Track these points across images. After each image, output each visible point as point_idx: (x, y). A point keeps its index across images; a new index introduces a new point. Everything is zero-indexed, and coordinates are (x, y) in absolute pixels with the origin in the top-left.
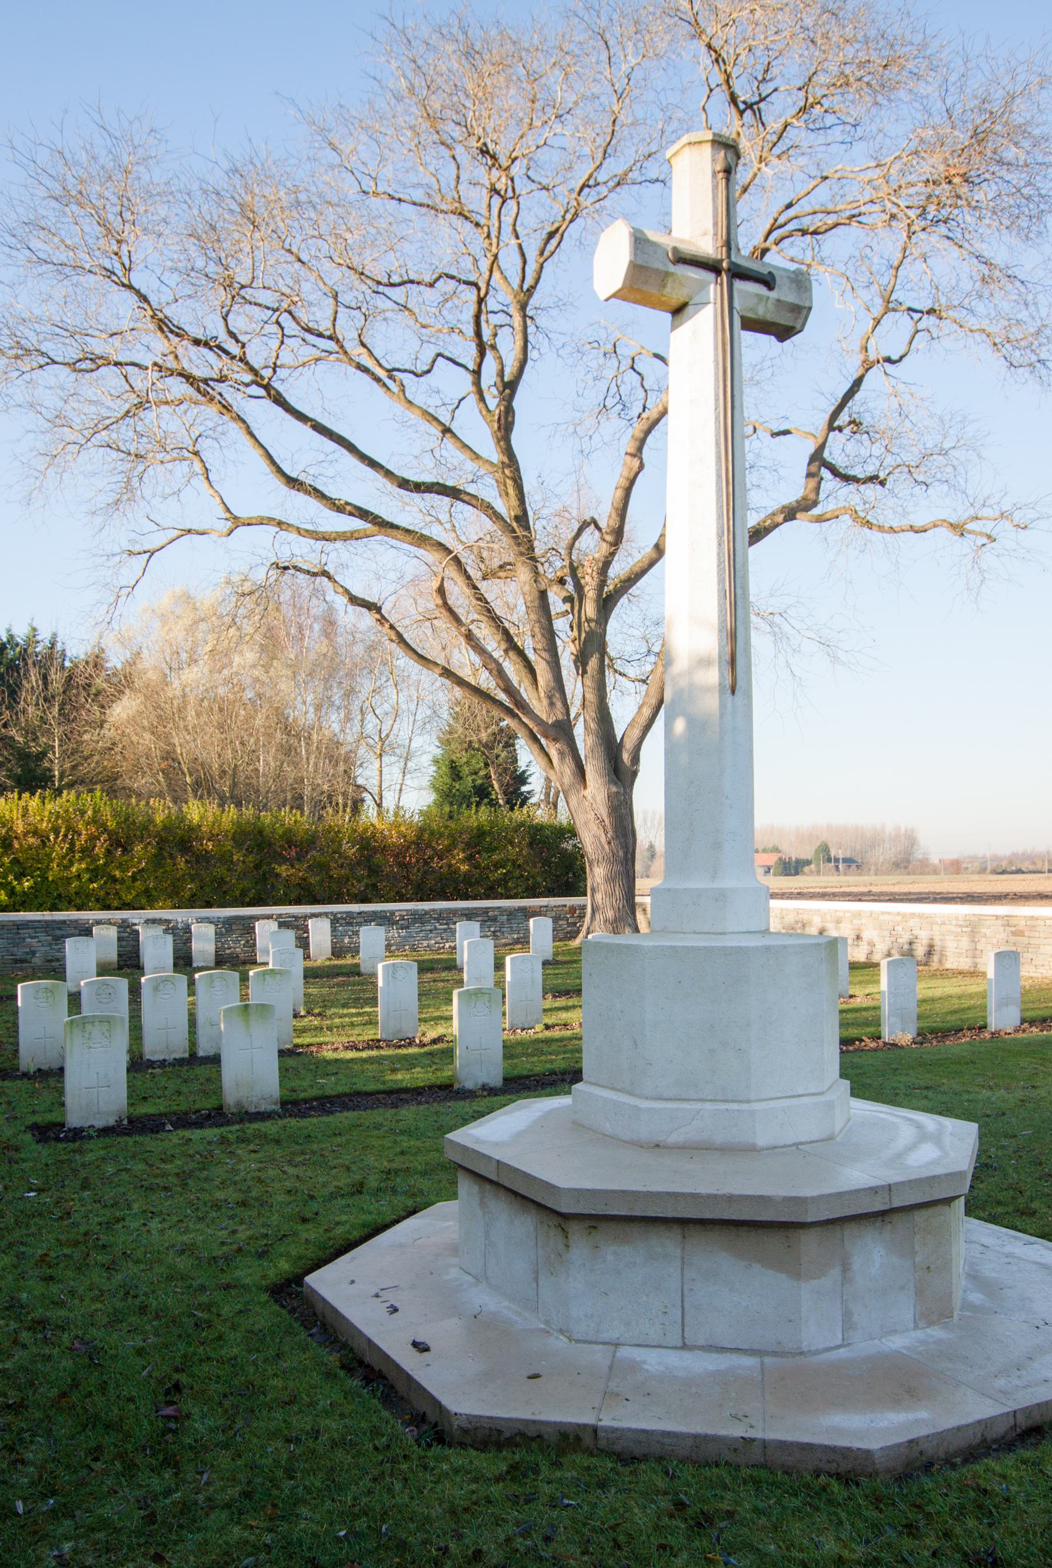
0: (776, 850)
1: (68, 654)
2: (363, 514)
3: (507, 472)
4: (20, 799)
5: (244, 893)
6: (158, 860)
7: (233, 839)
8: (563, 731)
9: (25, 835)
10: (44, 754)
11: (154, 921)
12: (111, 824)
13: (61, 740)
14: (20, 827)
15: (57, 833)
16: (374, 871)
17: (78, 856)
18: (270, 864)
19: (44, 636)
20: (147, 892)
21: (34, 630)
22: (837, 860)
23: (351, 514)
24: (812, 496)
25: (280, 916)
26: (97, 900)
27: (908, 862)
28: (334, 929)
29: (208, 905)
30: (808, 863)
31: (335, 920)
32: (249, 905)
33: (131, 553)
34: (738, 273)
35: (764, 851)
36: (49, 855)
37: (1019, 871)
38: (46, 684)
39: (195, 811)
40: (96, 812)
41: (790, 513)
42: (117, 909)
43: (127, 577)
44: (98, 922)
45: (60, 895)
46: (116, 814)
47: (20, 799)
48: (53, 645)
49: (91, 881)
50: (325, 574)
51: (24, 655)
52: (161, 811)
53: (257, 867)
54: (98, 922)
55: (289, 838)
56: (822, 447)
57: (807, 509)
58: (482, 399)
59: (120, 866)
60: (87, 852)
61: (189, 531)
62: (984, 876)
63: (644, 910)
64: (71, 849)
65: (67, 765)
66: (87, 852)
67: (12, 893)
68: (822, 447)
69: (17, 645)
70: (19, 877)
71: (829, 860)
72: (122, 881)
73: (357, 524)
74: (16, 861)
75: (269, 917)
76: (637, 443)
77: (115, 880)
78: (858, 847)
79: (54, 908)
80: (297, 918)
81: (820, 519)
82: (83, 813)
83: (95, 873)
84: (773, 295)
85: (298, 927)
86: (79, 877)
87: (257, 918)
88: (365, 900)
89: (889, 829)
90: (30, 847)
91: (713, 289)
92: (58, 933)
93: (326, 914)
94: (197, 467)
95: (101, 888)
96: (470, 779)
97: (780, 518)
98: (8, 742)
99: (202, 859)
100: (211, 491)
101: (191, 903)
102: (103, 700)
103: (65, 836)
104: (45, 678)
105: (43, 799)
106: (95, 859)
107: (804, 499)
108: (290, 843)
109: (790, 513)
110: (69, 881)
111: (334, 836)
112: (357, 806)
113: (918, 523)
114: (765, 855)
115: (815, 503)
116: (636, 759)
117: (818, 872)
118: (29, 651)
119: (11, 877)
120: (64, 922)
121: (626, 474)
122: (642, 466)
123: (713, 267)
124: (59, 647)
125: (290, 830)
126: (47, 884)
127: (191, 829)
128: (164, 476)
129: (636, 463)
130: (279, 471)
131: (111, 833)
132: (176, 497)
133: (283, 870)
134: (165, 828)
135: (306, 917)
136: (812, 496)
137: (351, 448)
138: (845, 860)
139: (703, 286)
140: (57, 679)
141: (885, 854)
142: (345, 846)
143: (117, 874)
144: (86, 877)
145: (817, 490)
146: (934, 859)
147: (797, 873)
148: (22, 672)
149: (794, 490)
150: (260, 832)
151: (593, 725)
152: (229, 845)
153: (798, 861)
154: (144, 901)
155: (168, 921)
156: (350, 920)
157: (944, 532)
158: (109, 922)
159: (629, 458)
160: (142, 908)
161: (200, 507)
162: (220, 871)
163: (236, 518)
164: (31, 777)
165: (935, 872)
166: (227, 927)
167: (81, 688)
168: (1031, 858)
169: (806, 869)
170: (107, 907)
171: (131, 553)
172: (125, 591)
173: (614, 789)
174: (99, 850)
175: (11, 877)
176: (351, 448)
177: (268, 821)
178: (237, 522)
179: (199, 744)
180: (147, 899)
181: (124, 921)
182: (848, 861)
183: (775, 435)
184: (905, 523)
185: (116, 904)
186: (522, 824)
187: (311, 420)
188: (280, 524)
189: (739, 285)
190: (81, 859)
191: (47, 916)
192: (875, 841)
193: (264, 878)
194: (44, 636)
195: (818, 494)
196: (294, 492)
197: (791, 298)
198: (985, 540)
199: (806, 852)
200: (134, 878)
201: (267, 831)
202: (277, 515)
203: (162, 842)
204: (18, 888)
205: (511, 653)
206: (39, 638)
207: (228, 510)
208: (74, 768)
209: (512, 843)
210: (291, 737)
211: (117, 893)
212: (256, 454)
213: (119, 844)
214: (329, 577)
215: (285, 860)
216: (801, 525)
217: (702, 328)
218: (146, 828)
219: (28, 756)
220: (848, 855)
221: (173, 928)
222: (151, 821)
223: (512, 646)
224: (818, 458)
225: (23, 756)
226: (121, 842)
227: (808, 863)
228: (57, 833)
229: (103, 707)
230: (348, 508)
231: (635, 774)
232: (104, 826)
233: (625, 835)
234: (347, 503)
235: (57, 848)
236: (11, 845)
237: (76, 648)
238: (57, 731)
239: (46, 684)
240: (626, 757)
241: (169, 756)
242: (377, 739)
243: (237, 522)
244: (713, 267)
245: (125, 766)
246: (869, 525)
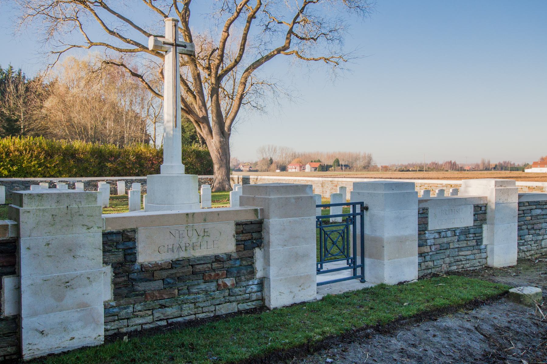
0: (319, 161)
1: (26, 77)
2: (137, 44)
3: (186, 33)
4: (12, 138)
5: (94, 172)
6: (63, 161)
7: (91, 154)
8: (205, 120)
9: (14, 151)
10: (17, 120)
11: (62, 181)
12: (46, 148)
13: (24, 113)
14: (12, 148)
15: (26, 150)
16: (141, 165)
17: (34, 159)
18: (104, 163)
19: (16, 69)
20: (59, 171)
21: (11, 67)
22: (342, 165)
23: (132, 44)
24: (287, 45)
25: (107, 180)
26: (41, 174)
27: (369, 166)
28: (126, 185)
29: (82, 176)
30: (331, 166)
31: (127, 182)
32: (96, 176)
33: (53, 52)
34: (177, 45)
35: (315, 161)
36: (23, 158)
37: (408, 171)
38: (17, 91)
39: (77, 144)
40: (41, 143)
41: (279, 51)
42: (48, 177)
43: (51, 61)
44: (42, 182)
45: (27, 173)
46: (47, 144)
47: (12, 138)
48: (19, 74)
49: (39, 167)
50: (122, 65)
51: (7, 78)
52: (64, 144)
53: (99, 164)
54: (42, 182)
55: (111, 154)
56: (292, 28)
57: (284, 50)
58: (177, 8)
59: (50, 163)
60: (37, 157)
61: (74, 46)
62: (395, 172)
63: (233, 180)
64: (31, 156)
65: (27, 123)
66: (37, 157)
67: (9, 171)
68: (292, 28)
69: (4, 73)
70: (12, 166)
71: (339, 166)
72: (50, 168)
73: (136, 47)
74: (11, 160)
75: (103, 181)
76: (226, 28)
77: (47, 167)
78: (350, 160)
79: (25, 177)
80: (113, 181)
81: (287, 54)
82: (36, 144)
83: (40, 165)
84: (186, 49)
85: (113, 183)
86: (34, 166)
87: (99, 181)
88: (138, 175)
89: (362, 154)
90: (16, 156)
91: (172, 49)
92: (27, 185)
93: (124, 180)
94: (77, 23)
95: (42, 170)
96: (188, 133)
97: (276, 53)
98: (2, 114)
99: (80, 160)
100: (83, 33)
101: (75, 176)
102: (42, 97)
103: (29, 152)
104: (16, 87)
105: (20, 138)
106: (40, 160)
107: (284, 46)
108: (112, 156)
109: (279, 51)
110: (31, 167)
111: (127, 153)
112: (147, 142)
113: (316, 58)
114: (315, 163)
115: (288, 48)
116: (230, 129)
117: (335, 170)
118: (10, 77)
119: (9, 166)
120: (29, 181)
121: (223, 37)
122: (228, 35)
123: (172, 45)
124: (22, 75)
125: (111, 151)
126: (20, 169)
127: (75, 150)
128: (64, 27)
129: (226, 34)
130: (107, 28)
131: (46, 151)
132: (68, 33)
133: (109, 165)
134: (66, 150)
135: (116, 181)
136: (287, 45)
137: (131, 23)
138: (345, 166)
139: (170, 48)
140: (22, 89)
141: (360, 163)
142: (131, 157)
143: (49, 165)
144: (37, 166)
145: (289, 43)
146: (379, 166)
147: (327, 171)
148: (7, 85)
149: (282, 43)
150: (101, 152)
151: (214, 119)
152: (89, 156)
153: (327, 166)
154: (58, 175)
155: (67, 181)
156: (132, 181)
157: (322, 61)
158: (46, 182)
159: (224, 33)
160: (58, 177)
161: (79, 38)
162: (86, 165)
163: (91, 42)
164: (12, 129)
165: (378, 170)
166: (87, 185)
167: (32, 92)
168: (413, 165)
169: (330, 169)
170: (45, 177)
171: (53, 52)
172: (50, 66)
173: (222, 140)
174: (42, 156)
175: (9, 166)
176: (131, 23)
177: (103, 148)
178: (92, 44)
179: (81, 117)
180: (59, 174)
181: (51, 181)
182: (346, 166)
183: (279, 23)
184: (312, 58)
185: (48, 175)
186: (194, 150)
187: (117, 14)
188: (107, 45)
189: (178, 48)
190: (35, 160)
191: (23, 179)
192: (357, 159)
193: (102, 168)
194: (16, 69)
195: (289, 45)
196: (112, 36)
197: (190, 49)
198: (335, 64)
199: (330, 162)
200: (55, 167)
201: (103, 151)
202: (107, 43)
203: (65, 155)
204: (12, 169)
205: (189, 93)
206: (13, 71)
207: (89, 40)
208: (29, 124)
209: (190, 157)
210: (118, 116)
211: (48, 172)
212: (99, 22)
213: (49, 155)
214: (125, 67)
215: (110, 161)
216: (282, 55)
217: (169, 58)
218: (59, 150)
219: (11, 120)
220: (346, 163)
221: (69, 184)
222: (61, 147)
223: (189, 90)
224: (291, 32)
225: (9, 120)
226: (50, 154)
227: (331, 166)
228: (26, 150)
229: (42, 100)
230: (131, 42)
231: (229, 135)
232: (43, 149)
233: (226, 155)
234: (131, 40)
235: (26, 156)
236: (9, 155)
237: (30, 75)
238: (23, 110)
239: (17, 91)
240: (226, 129)
241: (70, 120)
242: (154, 116)
243: (92, 44)
244: (172, 45)
245: (50, 124)
246: (301, 57)
